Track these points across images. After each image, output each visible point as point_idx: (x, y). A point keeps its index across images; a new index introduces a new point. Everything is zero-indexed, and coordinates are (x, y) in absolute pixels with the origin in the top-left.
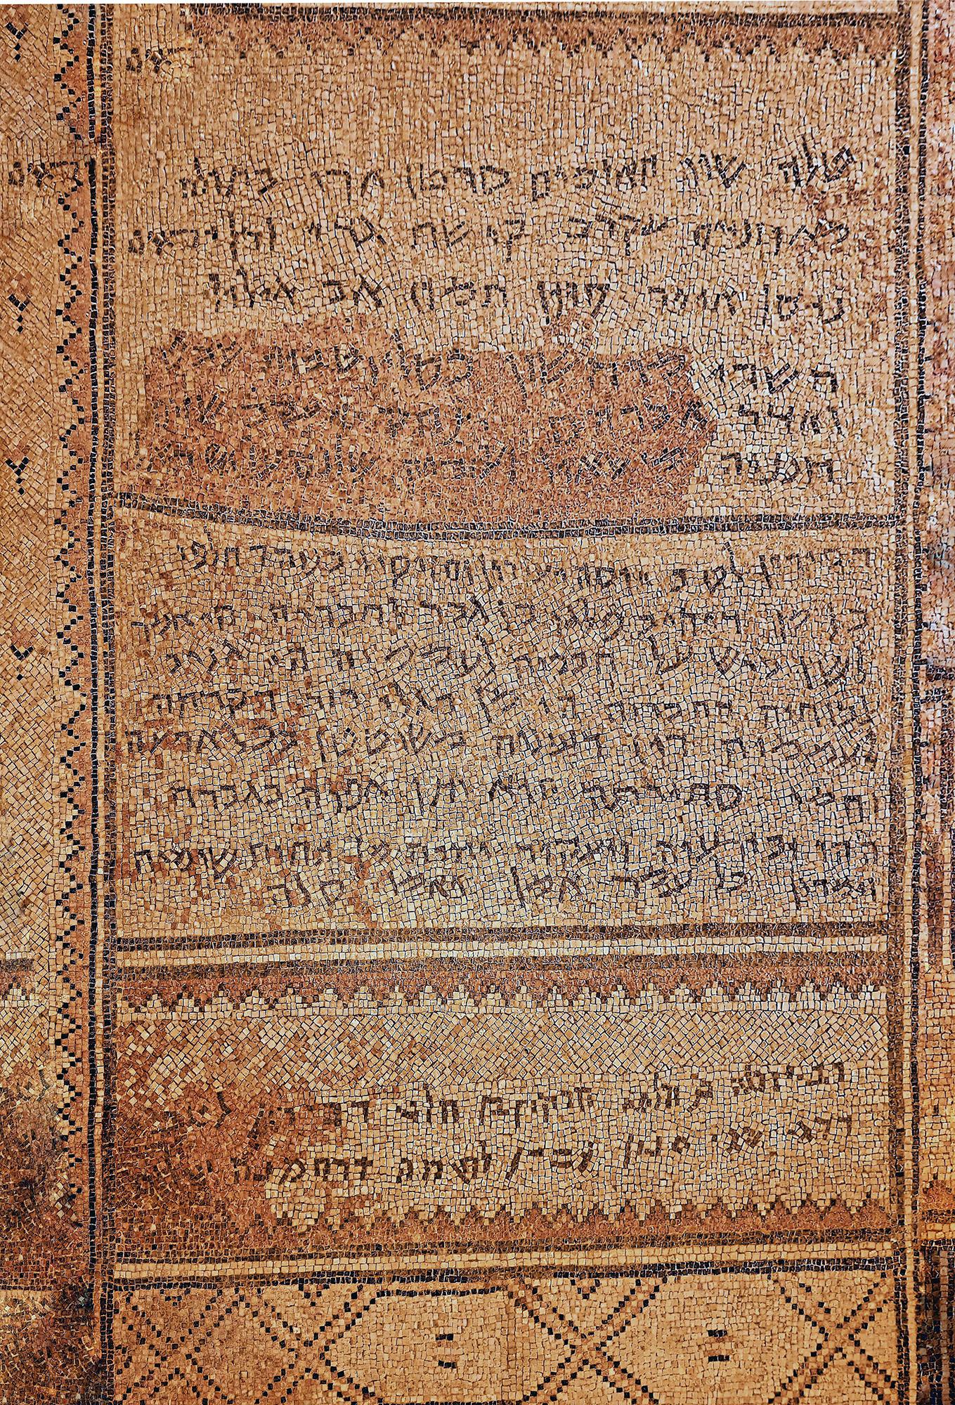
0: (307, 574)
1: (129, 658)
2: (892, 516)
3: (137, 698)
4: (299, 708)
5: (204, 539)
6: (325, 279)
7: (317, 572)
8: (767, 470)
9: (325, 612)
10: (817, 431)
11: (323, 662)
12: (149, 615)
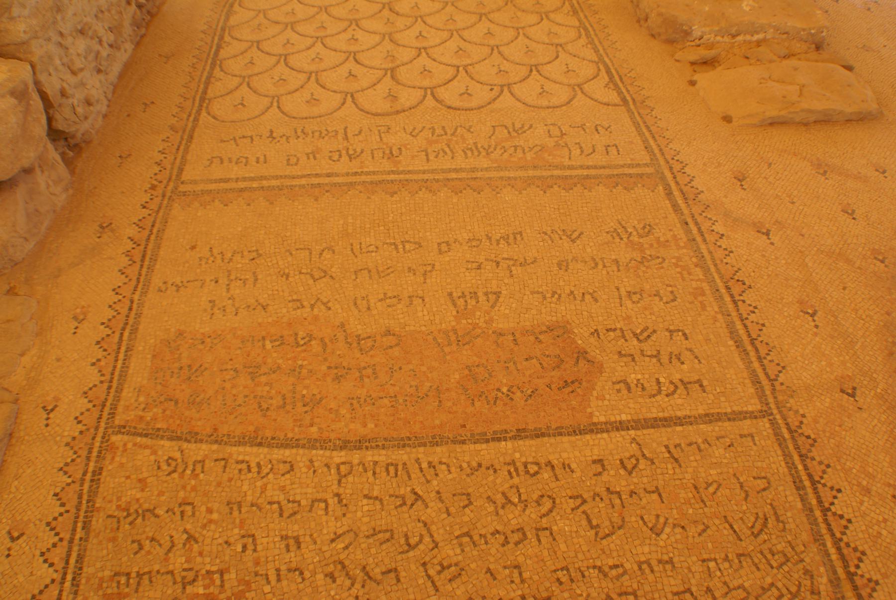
0: (263, 478)
1: (100, 543)
2: (761, 411)
3: (100, 575)
4: (248, 583)
5: (177, 455)
6: (290, 298)
7: (271, 476)
8: (652, 387)
9: (275, 506)
10: (683, 363)
11: (272, 545)
12: (124, 510)
